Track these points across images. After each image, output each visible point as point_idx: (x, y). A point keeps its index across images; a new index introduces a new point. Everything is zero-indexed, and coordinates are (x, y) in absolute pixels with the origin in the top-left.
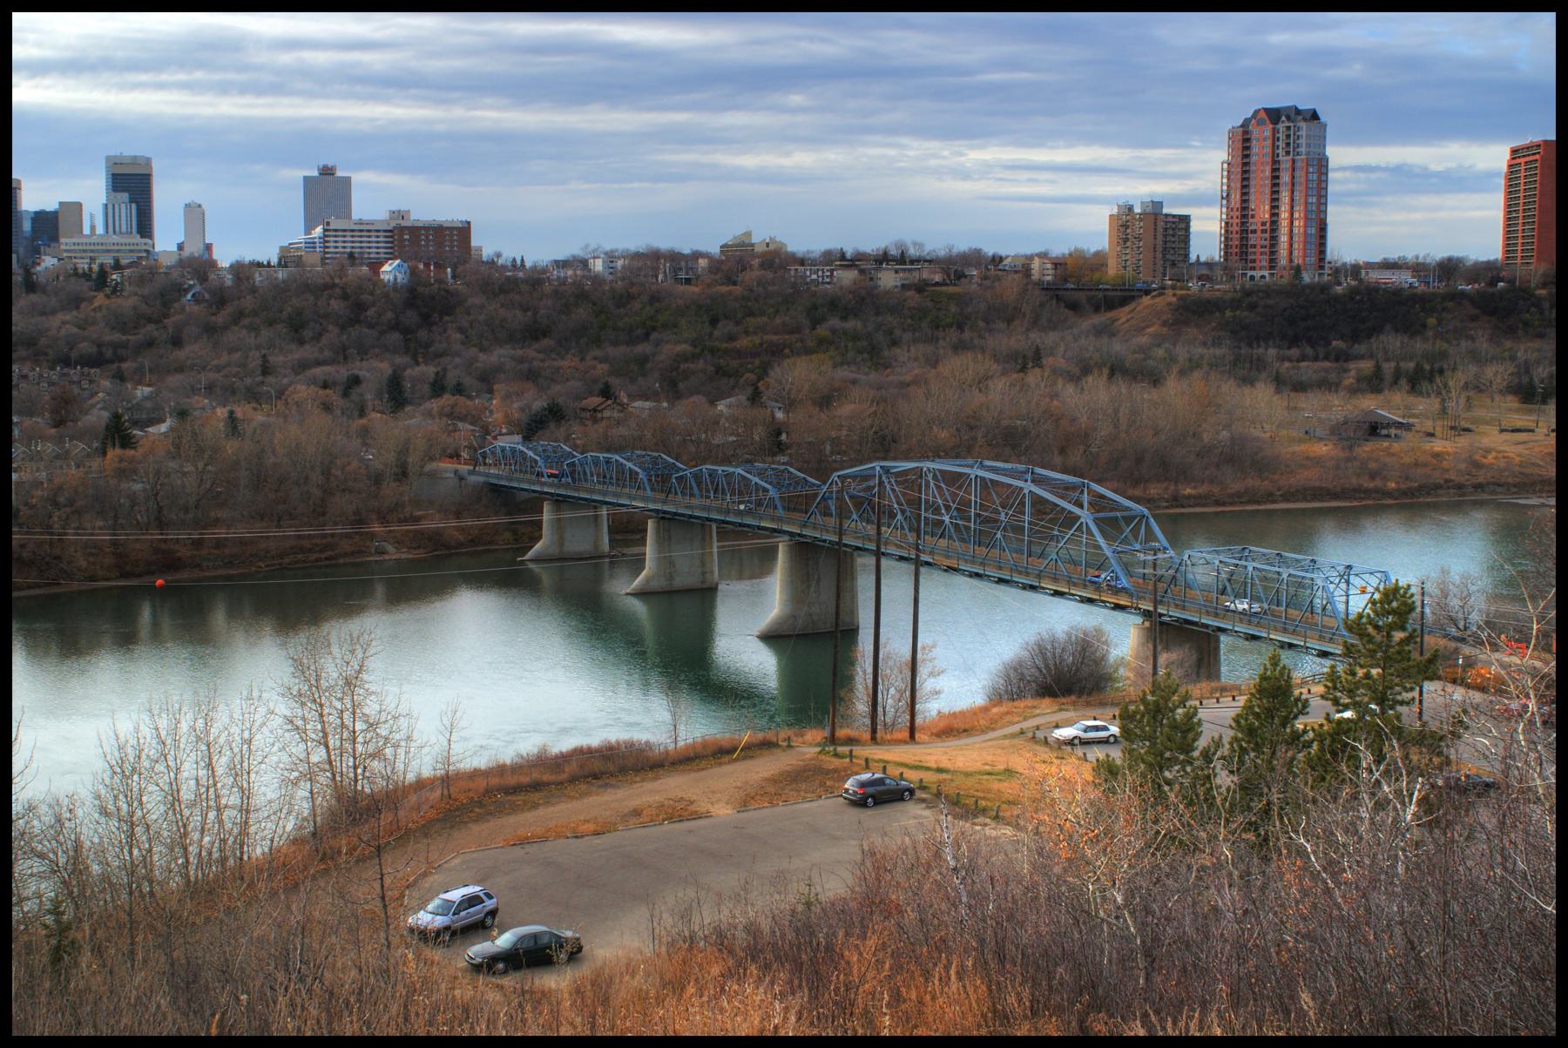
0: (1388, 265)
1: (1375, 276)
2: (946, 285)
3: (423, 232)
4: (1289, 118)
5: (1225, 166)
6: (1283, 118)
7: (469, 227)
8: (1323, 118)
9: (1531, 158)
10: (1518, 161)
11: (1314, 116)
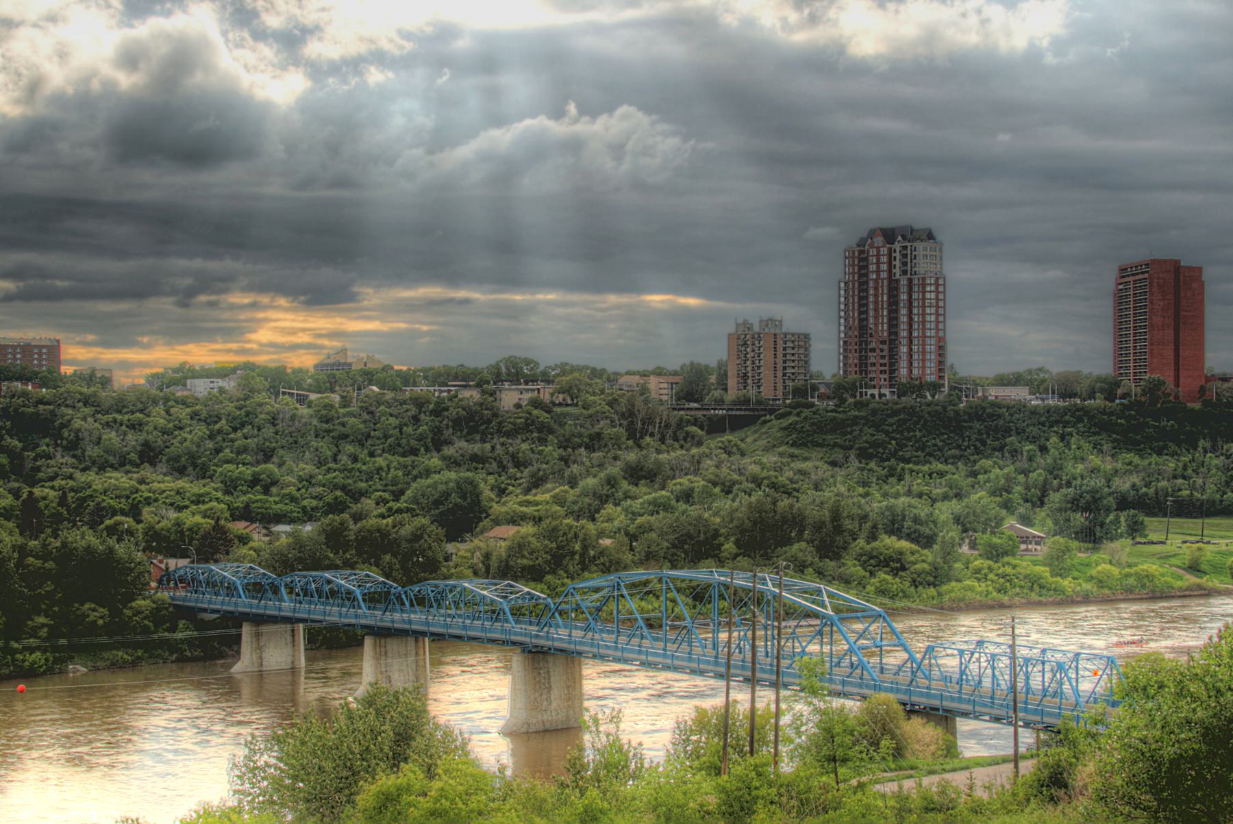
0: (1002, 381)
1: (993, 393)
2: (567, 405)
3: (36, 351)
4: (904, 237)
5: (842, 285)
6: (900, 238)
7: (59, 346)
8: (939, 237)
9: (1141, 276)
10: (1127, 279)
11: (930, 236)
